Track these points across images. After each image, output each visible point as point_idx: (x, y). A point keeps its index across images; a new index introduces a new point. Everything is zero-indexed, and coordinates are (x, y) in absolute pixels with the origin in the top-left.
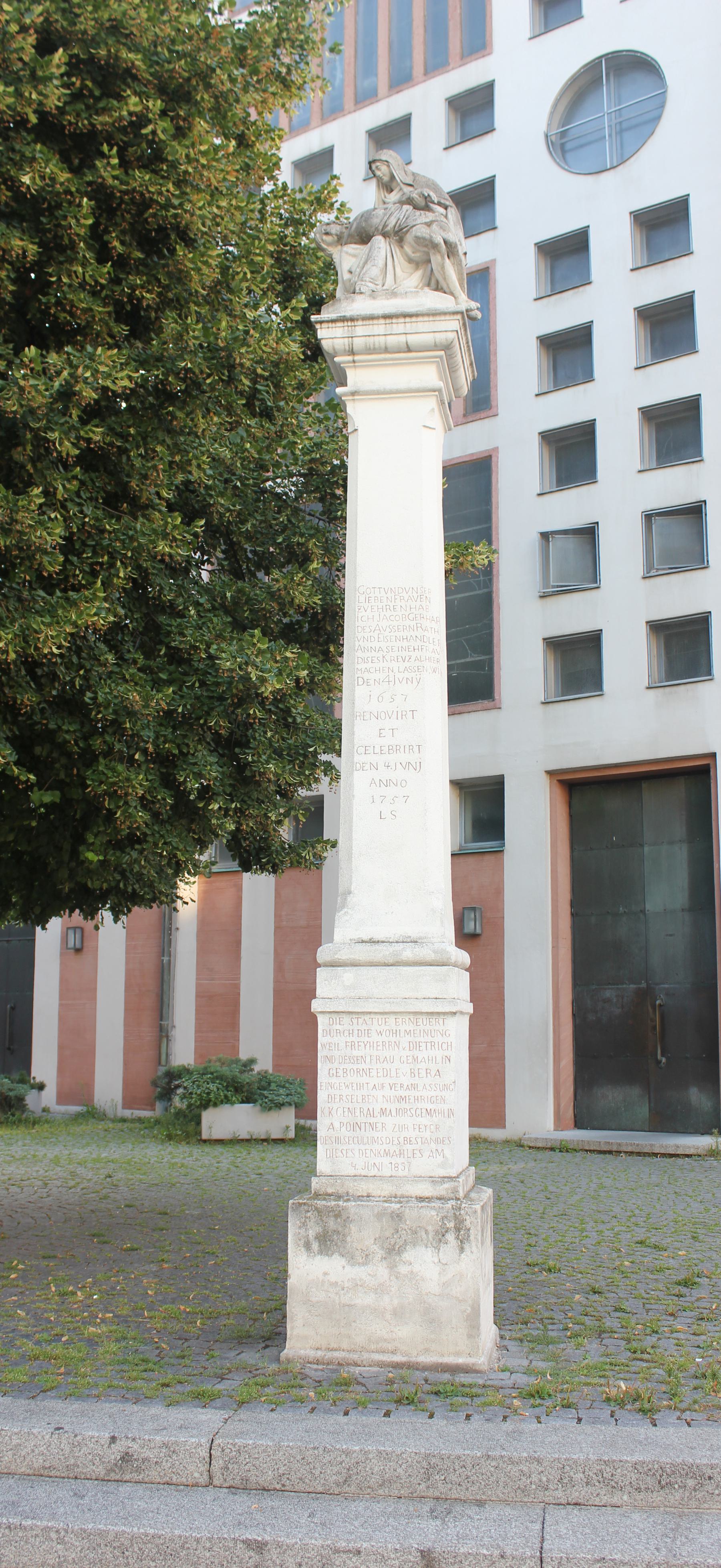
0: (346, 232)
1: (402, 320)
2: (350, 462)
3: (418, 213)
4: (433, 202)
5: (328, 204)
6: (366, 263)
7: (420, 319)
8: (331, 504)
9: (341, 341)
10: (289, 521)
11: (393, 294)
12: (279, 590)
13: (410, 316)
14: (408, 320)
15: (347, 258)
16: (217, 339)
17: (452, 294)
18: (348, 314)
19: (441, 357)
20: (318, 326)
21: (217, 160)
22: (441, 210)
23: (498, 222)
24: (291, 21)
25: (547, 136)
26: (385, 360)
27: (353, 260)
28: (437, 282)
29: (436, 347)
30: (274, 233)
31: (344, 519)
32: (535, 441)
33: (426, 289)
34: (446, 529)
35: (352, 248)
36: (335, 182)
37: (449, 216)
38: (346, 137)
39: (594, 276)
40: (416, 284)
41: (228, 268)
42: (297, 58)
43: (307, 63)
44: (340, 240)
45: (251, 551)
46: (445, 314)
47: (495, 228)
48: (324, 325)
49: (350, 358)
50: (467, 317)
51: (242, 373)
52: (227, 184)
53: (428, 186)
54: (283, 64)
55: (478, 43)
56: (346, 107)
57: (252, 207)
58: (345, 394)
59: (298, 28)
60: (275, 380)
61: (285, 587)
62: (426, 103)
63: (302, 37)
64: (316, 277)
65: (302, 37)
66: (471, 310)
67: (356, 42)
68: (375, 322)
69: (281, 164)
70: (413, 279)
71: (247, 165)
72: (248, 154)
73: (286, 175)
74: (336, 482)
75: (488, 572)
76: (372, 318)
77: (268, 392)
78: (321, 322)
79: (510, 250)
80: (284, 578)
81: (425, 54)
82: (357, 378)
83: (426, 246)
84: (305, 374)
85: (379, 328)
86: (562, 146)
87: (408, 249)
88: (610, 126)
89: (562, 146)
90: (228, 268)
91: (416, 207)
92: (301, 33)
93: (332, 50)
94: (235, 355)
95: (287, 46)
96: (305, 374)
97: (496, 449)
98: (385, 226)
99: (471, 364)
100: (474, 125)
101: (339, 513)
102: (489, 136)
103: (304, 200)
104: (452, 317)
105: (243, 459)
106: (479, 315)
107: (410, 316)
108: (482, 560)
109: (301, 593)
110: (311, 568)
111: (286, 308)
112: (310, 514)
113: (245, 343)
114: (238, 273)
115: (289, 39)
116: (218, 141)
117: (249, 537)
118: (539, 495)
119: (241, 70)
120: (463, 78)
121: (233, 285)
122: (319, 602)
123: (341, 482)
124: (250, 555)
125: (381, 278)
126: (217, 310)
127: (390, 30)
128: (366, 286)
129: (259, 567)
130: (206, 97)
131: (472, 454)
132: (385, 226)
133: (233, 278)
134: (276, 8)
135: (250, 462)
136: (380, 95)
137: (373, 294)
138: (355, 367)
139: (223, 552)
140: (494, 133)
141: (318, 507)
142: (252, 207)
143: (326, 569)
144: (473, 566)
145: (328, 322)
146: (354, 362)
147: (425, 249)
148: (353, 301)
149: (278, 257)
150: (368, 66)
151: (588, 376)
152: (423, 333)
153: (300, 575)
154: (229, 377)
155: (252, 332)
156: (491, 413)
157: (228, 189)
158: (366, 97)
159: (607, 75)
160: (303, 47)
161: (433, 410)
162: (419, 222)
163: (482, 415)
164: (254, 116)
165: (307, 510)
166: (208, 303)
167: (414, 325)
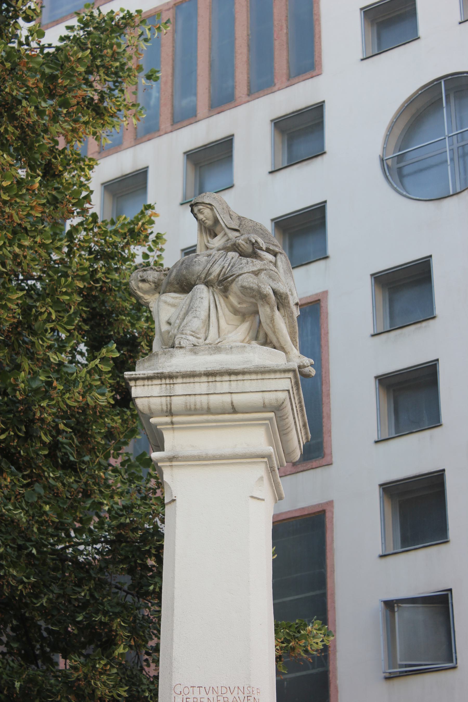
0: (165, 280)
1: (226, 378)
2: (166, 529)
3: (244, 260)
4: (261, 249)
5: (142, 237)
6: (186, 314)
7: (247, 377)
8: (142, 577)
9: (158, 400)
10: (92, 595)
11: (216, 349)
12: (78, 679)
13: (236, 373)
14: (233, 378)
15: (165, 309)
16: (15, 390)
17: (282, 349)
18: (166, 370)
19: (270, 419)
20: (132, 383)
21: (21, 197)
22: (270, 257)
23: (330, 251)
24: (105, 47)
25: (382, 160)
26: (208, 421)
27: (173, 310)
28: (266, 335)
29: (265, 408)
30: (84, 269)
31: (158, 595)
32: (374, 497)
33: (254, 343)
34: (274, 598)
35: (171, 297)
36: (149, 212)
37: (279, 263)
38: (162, 160)
39: (438, 310)
40: (242, 337)
41: (30, 308)
42: (111, 85)
43: (122, 91)
44: (158, 288)
45: (47, 629)
46: (275, 371)
47: (327, 258)
48: (139, 383)
49: (168, 419)
50: (300, 375)
51: (42, 428)
52: (31, 220)
53: (255, 231)
54: (95, 90)
55: (306, 63)
56: (162, 127)
57: (59, 244)
58: (162, 460)
59: (113, 56)
60: (81, 431)
61: (86, 676)
62: (250, 125)
63: (118, 64)
64: (128, 315)
65: (118, 64)
66: (305, 367)
67: (173, 60)
68: (197, 379)
69: (92, 197)
70: (238, 333)
71: (55, 198)
72: (56, 185)
73: (96, 205)
74: (149, 552)
75: (324, 656)
76: (193, 375)
77: (70, 445)
78: (136, 379)
79: (344, 281)
80: (84, 665)
81: (248, 74)
82: (175, 441)
83: (253, 297)
84: (115, 422)
85: (201, 386)
86: (400, 170)
87: (233, 299)
88: (452, 150)
89: (400, 170)
90: (30, 308)
91: (242, 254)
92: (116, 60)
93: (149, 77)
94: (35, 408)
95: (101, 73)
96: (115, 422)
97: (331, 503)
98: (208, 274)
99: (304, 425)
100: (302, 148)
101: (151, 588)
102: (319, 159)
103: (116, 232)
104: (283, 375)
105: (41, 523)
106: (313, 372)
107: (236, 373)
108: (316, 644)
109: (104, 683)
110: (116, 653)
111: (95, 358)
112: (117, 587)
113: (46, 396)
114: (41, 313)
115: (103, 66)
116: (22, 173)
117: (45, 613)
118: (382, 556)
119: (50, 102)
120: (291, 98)
121: (36, 326)
122: (125, 695)
123: (153, 551)
124: (45, 634)
125: (203, 331)
126: (17, 354)
127: (210, 49)
128: (187, 340)
129: (55, 649)
130: (10, 129)
131: (303, 509)
132: (208, 274)
133: (36, 319)
134: (89, 33)
135: (48, 526)
136: (199, 116)
137: (195, 349)
138: (173, 429)
139: (13, 629)
140: (325, 156)
141: (126, 580)
142: (59, 244)
143: (133, 653)
144: (306, 651)
145: (143, 379)
146: (172, 423)
147: (253, 300)
148: (172, 356)
149: (87, 296)
150: (186, 84)
151: (435, 421)
152: (250, 392)
153: (103, 662)
154: (26, 433)
155: (55, 383)
156: (323, 461)
157: (32, 225)
158: (184, 117)
159: (447, 97)
160: (118, 75)
161: (261, 478)
162: (246, 270)
163: (314, 464)
164: (62, 144)
165: (113, 582)
166: (8, 345)
167: (240, 383)
